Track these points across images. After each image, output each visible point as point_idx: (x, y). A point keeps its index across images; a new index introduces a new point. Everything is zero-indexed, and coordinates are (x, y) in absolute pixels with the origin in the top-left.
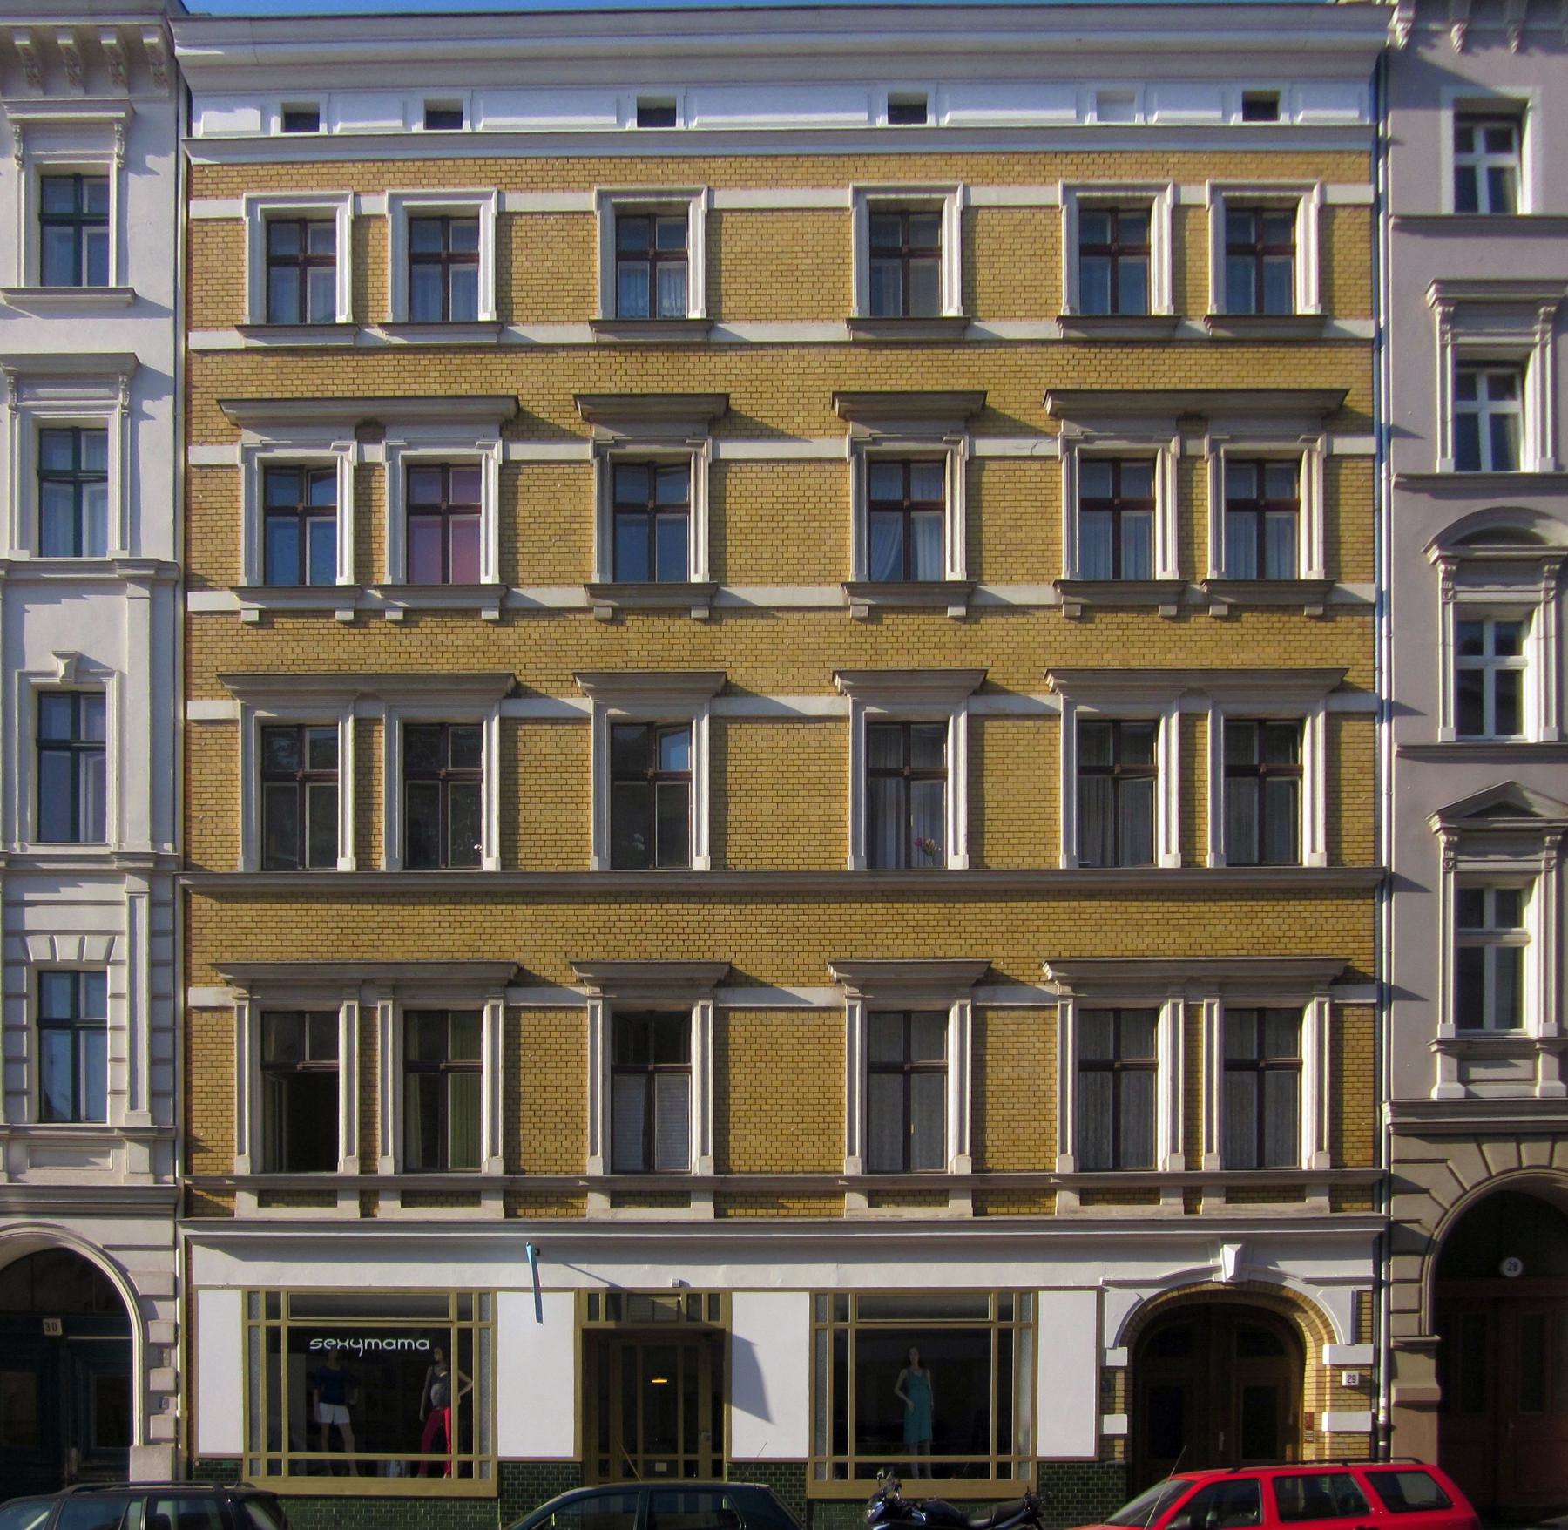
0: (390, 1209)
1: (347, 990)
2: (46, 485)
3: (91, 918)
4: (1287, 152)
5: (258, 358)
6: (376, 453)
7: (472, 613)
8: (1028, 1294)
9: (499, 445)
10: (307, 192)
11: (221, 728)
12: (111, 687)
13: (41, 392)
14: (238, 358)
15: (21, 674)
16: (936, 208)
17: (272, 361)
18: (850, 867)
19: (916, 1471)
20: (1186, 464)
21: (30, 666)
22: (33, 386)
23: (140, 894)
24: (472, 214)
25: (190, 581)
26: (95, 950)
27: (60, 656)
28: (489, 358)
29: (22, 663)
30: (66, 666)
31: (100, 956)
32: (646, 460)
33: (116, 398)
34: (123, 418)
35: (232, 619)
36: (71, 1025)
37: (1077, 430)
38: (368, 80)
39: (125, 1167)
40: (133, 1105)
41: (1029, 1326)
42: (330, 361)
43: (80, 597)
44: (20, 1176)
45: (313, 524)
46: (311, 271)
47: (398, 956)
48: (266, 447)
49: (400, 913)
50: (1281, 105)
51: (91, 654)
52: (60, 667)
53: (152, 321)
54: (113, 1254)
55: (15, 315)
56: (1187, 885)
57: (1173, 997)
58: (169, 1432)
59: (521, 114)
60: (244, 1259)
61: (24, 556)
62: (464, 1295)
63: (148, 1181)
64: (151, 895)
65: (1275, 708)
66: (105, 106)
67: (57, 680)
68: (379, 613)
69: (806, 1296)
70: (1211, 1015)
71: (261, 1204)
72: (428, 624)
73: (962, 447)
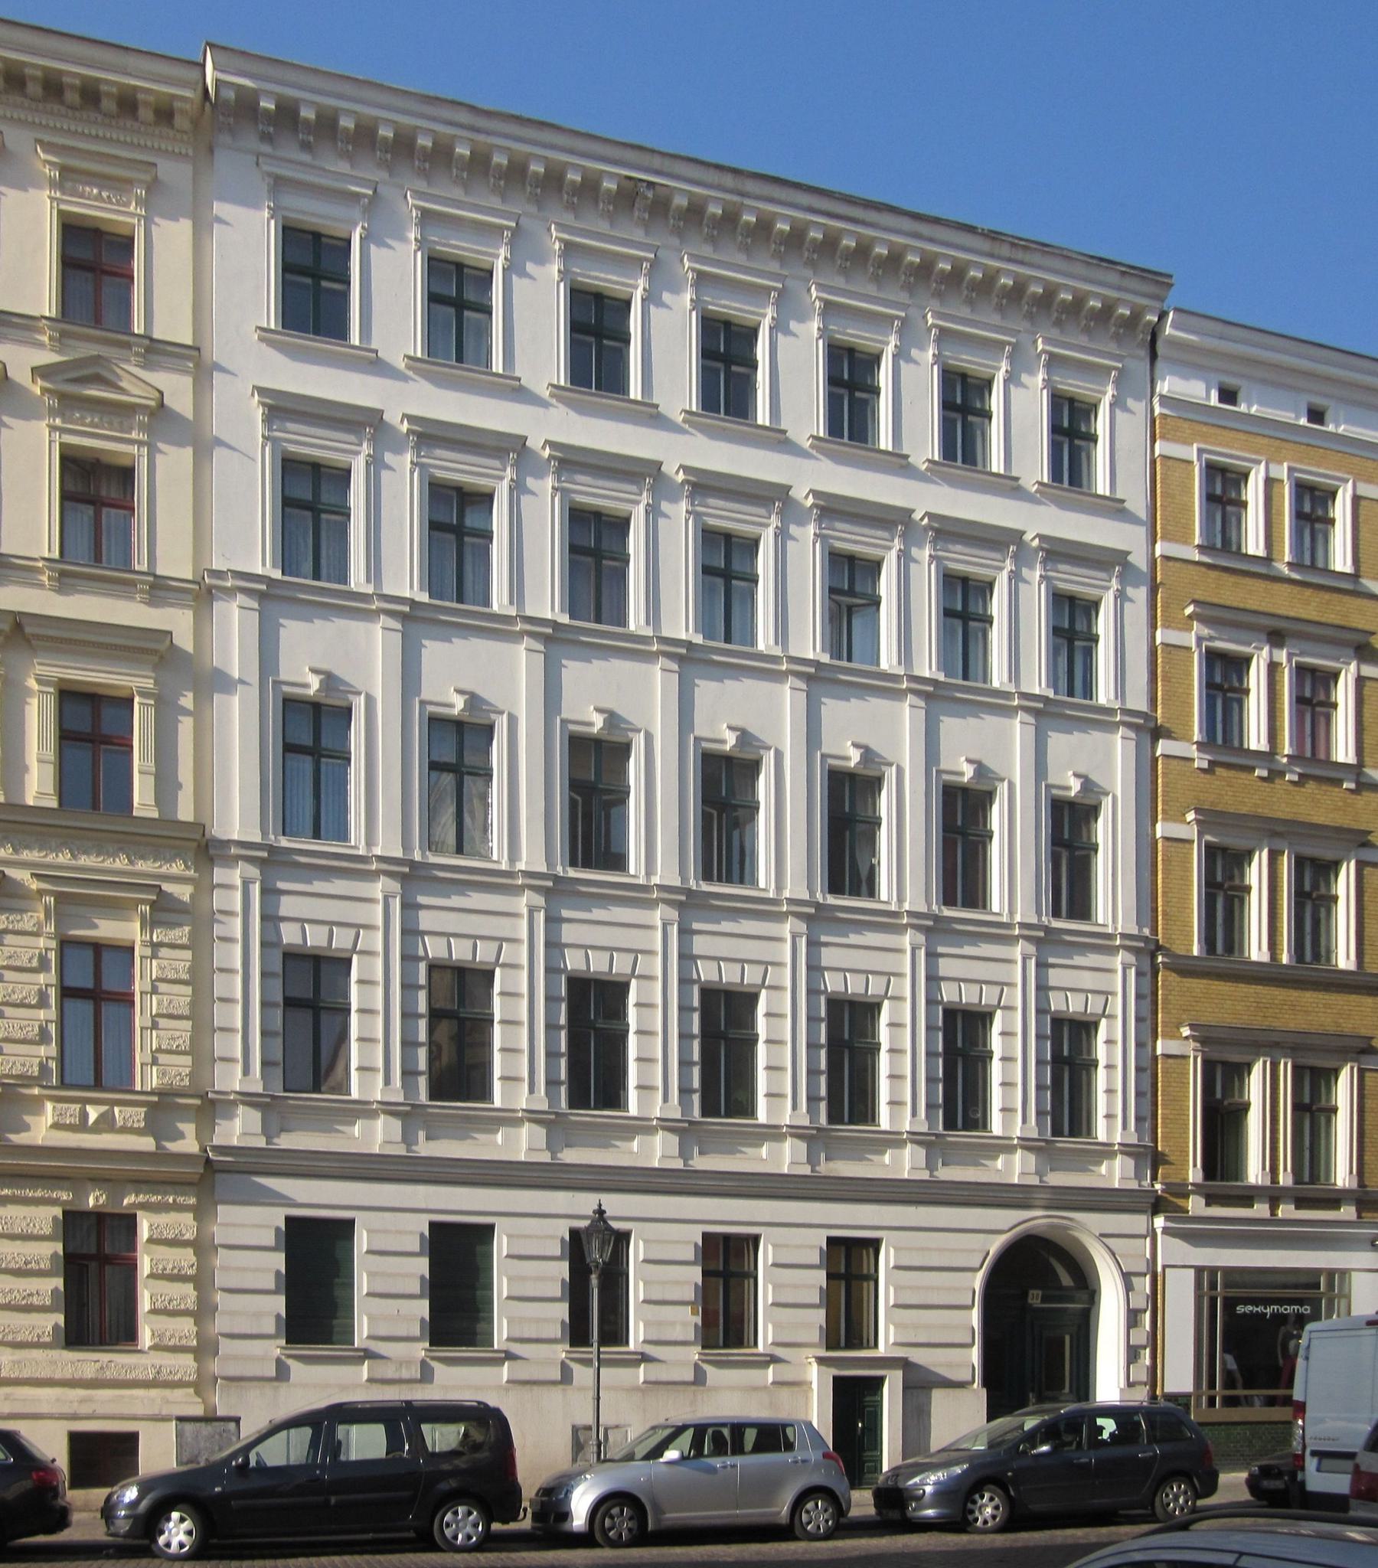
0: (1286, 1211)
1: (1262, 1050)
2: (288, 510)
3: (1087, 980)
4: (1225, 428)
5: (1203, 569)
6: (1282, 656)
7: (1338, 782)
8: (1344, 1273)
9: (1266, 649)
10: (1234, 452)
11: (1180, 845)
12: (359, 705)
14: (1191, 567)
15: (274, 682)
17: (1213, 574)
18: (1195, 953)
19: (1243, 1400)
20: (1273, 668)
22: (705, 496)
23: (1130, 966)
25: (1157, 733)
28: (1346, 599)
29: (938, 763)
30: (321, 682)
31: (349, 946)
35: (1188, 764)
36: (1070, 1062)
37: (1206, 632)
38: (1279, 379)
39: (1116, 1173)
40: (246, 1071)
41: (1341, 1296)
42: (1248, 581)
43: (1085, 732)
44: (276, 1140)
47: (1292, 1027)
48: (1211, 638)
49: (1294, 994)
50: (1241, 396)
51: (337, 672)
53: (799, 460)
54: (1109, 1241)
55: (1039, 503)
56: (1267, 975)
57: (1265, 1055)
58: (1144, 1377)
59: (1365, 427)
60: (1196, 1246)
62: (1331, 1273)
65: (1324, 852)
66: (1102, 352)
67: (311, 692)
68: (1282, 774)
69: (1192, 1271)
70: (1285, 1069)
71: (1208, 1204)
72: (1311, 786)
73: (1353, 666)
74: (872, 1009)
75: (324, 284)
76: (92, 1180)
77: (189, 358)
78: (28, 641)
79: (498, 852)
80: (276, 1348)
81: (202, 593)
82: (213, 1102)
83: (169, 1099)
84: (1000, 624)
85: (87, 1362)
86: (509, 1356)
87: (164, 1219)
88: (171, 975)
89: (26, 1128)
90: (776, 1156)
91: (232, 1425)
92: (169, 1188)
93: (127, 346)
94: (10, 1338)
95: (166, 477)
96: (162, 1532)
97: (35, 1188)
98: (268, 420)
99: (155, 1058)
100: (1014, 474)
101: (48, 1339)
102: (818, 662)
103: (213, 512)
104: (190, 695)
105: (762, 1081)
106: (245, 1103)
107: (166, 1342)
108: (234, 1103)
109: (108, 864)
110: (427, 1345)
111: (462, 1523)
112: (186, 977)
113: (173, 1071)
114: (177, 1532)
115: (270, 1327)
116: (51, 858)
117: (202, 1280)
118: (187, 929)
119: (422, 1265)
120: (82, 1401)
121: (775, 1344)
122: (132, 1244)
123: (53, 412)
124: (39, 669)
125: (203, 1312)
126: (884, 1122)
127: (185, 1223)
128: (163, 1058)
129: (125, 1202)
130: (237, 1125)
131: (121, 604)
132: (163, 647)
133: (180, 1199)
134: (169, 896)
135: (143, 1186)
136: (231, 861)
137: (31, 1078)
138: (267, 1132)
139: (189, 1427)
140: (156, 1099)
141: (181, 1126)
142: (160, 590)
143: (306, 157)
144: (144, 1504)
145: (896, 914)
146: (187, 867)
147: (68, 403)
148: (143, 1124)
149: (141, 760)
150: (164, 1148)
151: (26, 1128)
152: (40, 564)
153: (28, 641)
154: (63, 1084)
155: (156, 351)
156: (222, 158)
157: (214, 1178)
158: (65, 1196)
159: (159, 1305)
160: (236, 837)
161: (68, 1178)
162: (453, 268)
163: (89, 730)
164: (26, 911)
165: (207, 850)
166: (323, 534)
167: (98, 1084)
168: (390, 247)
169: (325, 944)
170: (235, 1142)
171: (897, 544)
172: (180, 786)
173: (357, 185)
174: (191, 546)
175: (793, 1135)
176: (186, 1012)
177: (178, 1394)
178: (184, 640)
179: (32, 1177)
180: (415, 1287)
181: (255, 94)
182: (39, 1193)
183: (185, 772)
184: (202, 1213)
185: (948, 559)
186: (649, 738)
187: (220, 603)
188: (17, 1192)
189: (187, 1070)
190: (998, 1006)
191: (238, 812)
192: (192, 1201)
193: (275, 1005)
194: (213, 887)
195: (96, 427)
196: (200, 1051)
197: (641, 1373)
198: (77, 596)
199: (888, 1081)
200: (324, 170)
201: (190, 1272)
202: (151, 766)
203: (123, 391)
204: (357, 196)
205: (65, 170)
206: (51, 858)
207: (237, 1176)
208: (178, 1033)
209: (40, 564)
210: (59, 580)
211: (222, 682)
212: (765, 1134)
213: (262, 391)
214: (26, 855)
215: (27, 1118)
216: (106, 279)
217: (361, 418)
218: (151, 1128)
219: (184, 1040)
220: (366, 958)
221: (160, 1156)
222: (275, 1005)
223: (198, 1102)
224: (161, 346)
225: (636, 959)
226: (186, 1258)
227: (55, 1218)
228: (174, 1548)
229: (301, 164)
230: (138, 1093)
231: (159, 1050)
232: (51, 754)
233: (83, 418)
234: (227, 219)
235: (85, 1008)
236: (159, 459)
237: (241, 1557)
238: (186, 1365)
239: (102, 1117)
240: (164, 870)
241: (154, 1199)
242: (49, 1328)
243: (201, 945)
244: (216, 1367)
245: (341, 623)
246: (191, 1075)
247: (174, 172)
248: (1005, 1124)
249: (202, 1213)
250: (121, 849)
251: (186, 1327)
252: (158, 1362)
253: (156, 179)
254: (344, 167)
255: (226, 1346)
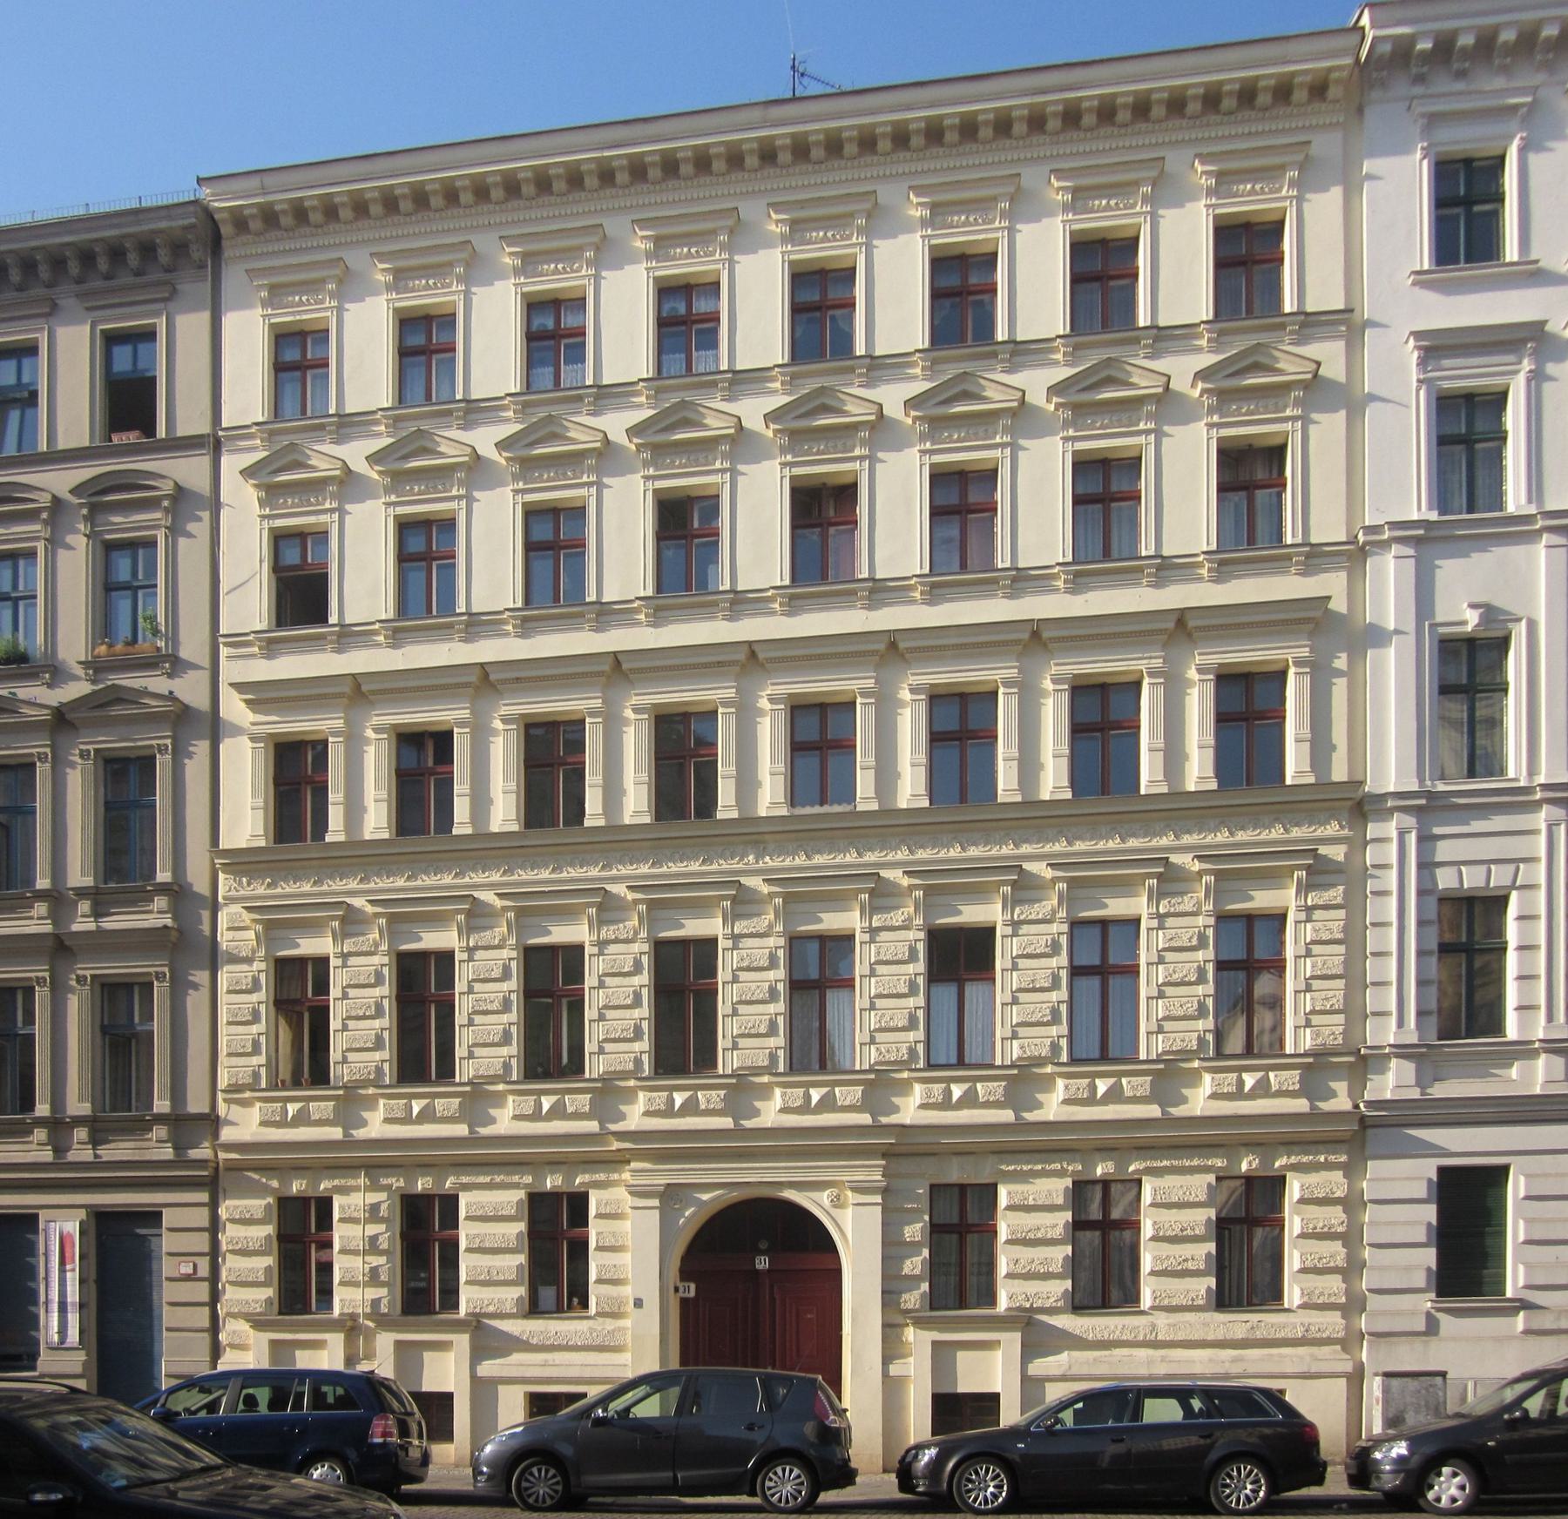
12: (1519, 634)
13: (1446, 363)
15: (1431, 626)
16: (850, 265)
21: (1439, 619)
24: (322, 327)
26: (1499, 877)
27: (1473, 606)
29: (1432, 614)
32: (1101, 457)
33: (1520, 363)
34: (1529, 381)
40: (1401, 1023)
44: (1429, 1091)
45: (439, 567)
46: (435, 358)
51: (1497, 603)
52: (1472, 619)
61: (1434, 516)
63: (1415, 1094)
64: (1419, 830)
74: (1498, 903)
75: (1477, 208)
76: (1246, 1145)
77: (1340, 322)
78: (903, 655)
79: (1515, 766)
80: (1427, 1302)
81: (1353, 555)
82: (1364, 1058)
83: (1323, 1060)
84: (1516, 441)
85: (1237, 1323)
86: (1525, 1305)
87: (1313, 1178)
88: (1325, 936)
89: (1184, 1100)
90: (1528, 1076)
91: (1439, 1380)
92: (1321, 1147)
93: (994, 355)
94: (1166, 1302)
95: (1317, 450)
96: (1431, 1487)
97: (1191, 1158)
98: (1422, 363)
99: (1304, 1017)
100: (1533, 257)
101: (1201, 1302)
102: (1427, 521)
103: (1366, 468)
104: (1344, 656)
105: (1512, 994)
106: (1398, 1056)
107: (1315, 1300)
108: (1388, 1057)
109: (1265, 835)
110: (1433, 1295)
111: (786, 1482)
112: (1339, 936)
113: (1327, 1031)
114: (1450, 1487)
115: (1420, 1280)
116: (1210, 839)
117: (1351, 1238)
118: (1341, 888)
119: (1430, 1213)
120: (1235, 1360)
121: (1527, 1287)
122: (1279, 1207)
123: (923, 438)
124: (914, 680)
125: (1352, 1269)
126: (1512, 1031)
127: (1335, 1183)
128: (1315, 1019)
129: (1277, 1164)
130: (1390, 1078)
131: (445, 646)
132: (1318, 614)
133: (1332, 1158)
134: (748, 889)
135: (1295, 1148)
136: (1385, 815)
137: (902, 1062)
138: (1421, 1083)
139: (1395, 1382)
140: (1311, 1060)
141: (1333, 1085)
142: (1315, 557)
143: (1460, 86)
144: (1416, 1460)
145: (1527, 790)
146: (1342, 827)
147: (399, 479)
148: (1297, 1087)
149: (864, 756)
150: (1317, 1108)
151: (1184, 1100)
152: (377, 626)
153: (1190, 635)
154: (930, 1066)
155: (1311, 324)
156: (1371, 114)
157: (1367, 1134)
158: (1219, 1163)
159: (1309, 1264)
160: (1392, 789)
161: (527, 1164)
162: (1461, 165)
163: (956, 727)
164: (1186, 893)
165: (1360, 806)
166: (1479, 464)
167: (1104, 1057)
168: (1551, 150)
169: (1456, 885)
170: (1388, 1096)
171: (1527, 365)
172: (1334, 748)
173: (1514, 96)
174: (1344, 508)
175: (1547, 1051)
176: (1340, 970)
177: (1326, 1351)
178: (1339, 605)
179: (521, 1164)
180: (1420, 1235)
181: (1412, 39)
182: (1195, 1162)
183: (1339, 735)
184: (1352, 1170)
185: (1440, 379)
186: (1532, 626)
187: (1375, 558)
188: (1175, 1163)
189: (1341, 1029)
190: (1513, 887)
191: (1392, 765)
192: (1343, 1158)
193: (1430, 953)
194: (1366, 843)
195: (685, 466)
196: (1354, 1012)
197: (1520, 1321)
198: (947, 605)
199: (1515, 984)
200: (1480, 92)
201: (1340, 1229)
202: (1160, 743)
203: (573, 441)
204: (1516, 107)
205: (1220, 175)
206: (1210, 839)
207: (1380, 1130)
208: (1331, 993)
209: (377, 626)
210: (930, 593)
211: (1376, 636)
212: (1516, 1051)
213: (1418, 335)
214: (1187, 839)
215: (758, 1104)
216: (1256, 268)
217: (1521, 335)
218: (1305, 1091)
219: (1338, 1000)
220: (1527, 893)
221: (1314, 1116)
222: (1430, 953)
223: (1352, 1059)
224: (1169, 332)
225: (1489, 871)
226: (1335, 1217)
227: (1209, 1185)
228: (1444, 1502)
229: (1460, 93)
230: (999, 1067)
231: (1313, 1012)
232: (922, 758)
233: (950, 436)
234: (1379, 174)
235: (1094, 982)
236: (1312, 429)
237: (1062, 1512)
238: (1332, 1323)
239: (966, 1093)
240: (1319, 833)
241: (1305, 1159)
242: (1203, 1292)
243: (1354, 905)
244: (1363, 1323)
245: (1499, 552)
246: (1344, 1033)
247: (1325, 145)
248: (1522, 1026)
249: (1352, 1170)
250: (850, 844)
251: (1334, 1286)
252: (1306, 1321)
253: (1019, 188)
254: (1499, 82)
255: (1374, 1302)
